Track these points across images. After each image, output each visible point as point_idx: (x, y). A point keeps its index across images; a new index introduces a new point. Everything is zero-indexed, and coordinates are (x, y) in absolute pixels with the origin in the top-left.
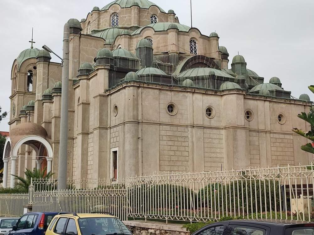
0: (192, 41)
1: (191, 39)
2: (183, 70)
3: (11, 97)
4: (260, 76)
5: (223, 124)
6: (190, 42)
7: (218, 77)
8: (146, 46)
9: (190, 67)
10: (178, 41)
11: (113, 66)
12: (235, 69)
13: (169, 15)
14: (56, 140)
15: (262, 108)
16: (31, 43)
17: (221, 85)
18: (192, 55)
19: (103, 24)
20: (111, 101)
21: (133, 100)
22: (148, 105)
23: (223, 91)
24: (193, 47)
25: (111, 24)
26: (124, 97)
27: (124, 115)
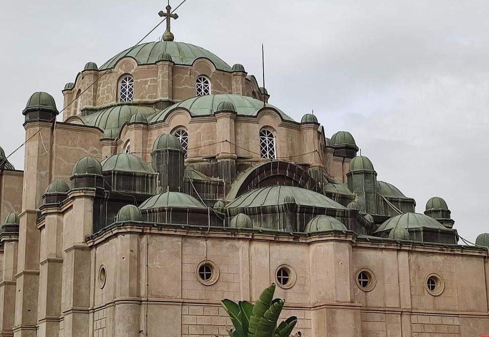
0: (265, 132)
1: (263, 129)
2: (243, 190)
4: (408, 195)
5: (311, 300)
6: (261, 134)
7: (302, 207)
8: (169, 148)
9: (257, 185)
10: (236, 134)
11: (103, 190)
12: (354, 184)
13: (234, 75)
15: (393, 268)
17: (308, 223)
18: (263, 161)
19: (105, 96)
20: (95, 258)
21: (130, 260)
22: (159, 267)
23: (310, 235)
24: (267, 145)
25: (120, 96)
26: (115, 252)
27: (115, 285)
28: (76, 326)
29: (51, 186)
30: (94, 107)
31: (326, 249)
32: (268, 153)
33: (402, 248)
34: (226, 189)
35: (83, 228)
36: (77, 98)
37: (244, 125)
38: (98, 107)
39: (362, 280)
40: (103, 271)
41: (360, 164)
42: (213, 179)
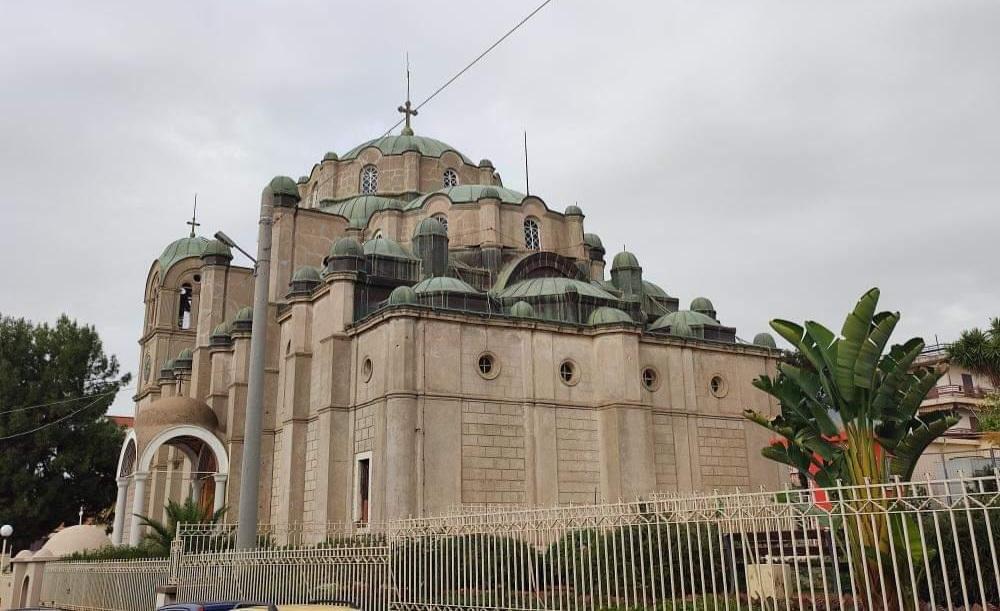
0: (529, 222)
2: (510, 282)
3: (144, 342)
4: (671, 294)
5: (597, 398)
7: (584, 297)
23: (595, 327)
26: (385, 340)
28: (334, 427)
33: (688, 345)
38: (339, 198)
40: (369, 361)
42: (476, 268)
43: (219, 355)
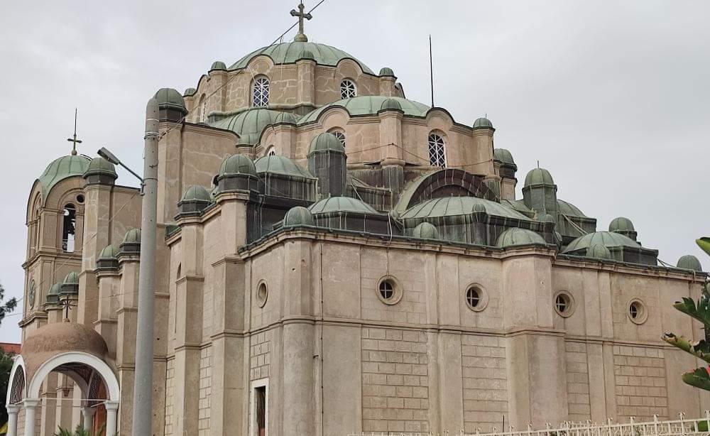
0: (434, 137)
1: (432, 133)
2: (414, 201)
3: (27, 266)
6: (430, 139)
7: (493, 217)
9: (430, 195)
10: (403, 137)
14: (128, 361)
16: (73, 143)
22: (335, 281)
23: (505, 249)
24: (437, 152)
26: (281, 263)
27: (282, 301)
29: (109, 248)
30: (224, 113)
31: (527, 265)
32: (438, 161)
33: (604, 268)
34: (394, 199)
35: (235, 237)
36: (200, 105)
37: (411, 128)
38: (228, 112)
39: (559, 304)
41: (539, 177)
43: (107, 279)
